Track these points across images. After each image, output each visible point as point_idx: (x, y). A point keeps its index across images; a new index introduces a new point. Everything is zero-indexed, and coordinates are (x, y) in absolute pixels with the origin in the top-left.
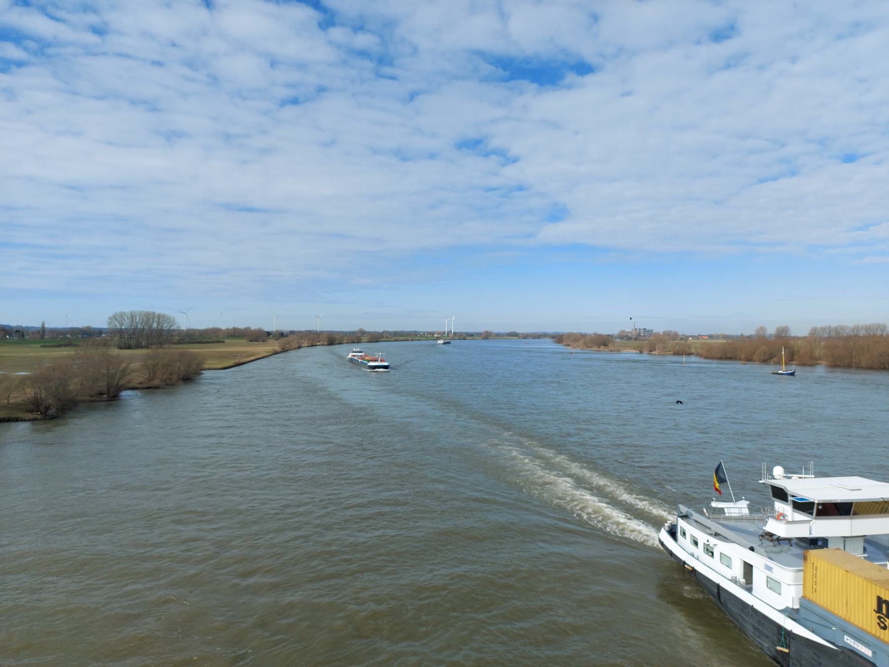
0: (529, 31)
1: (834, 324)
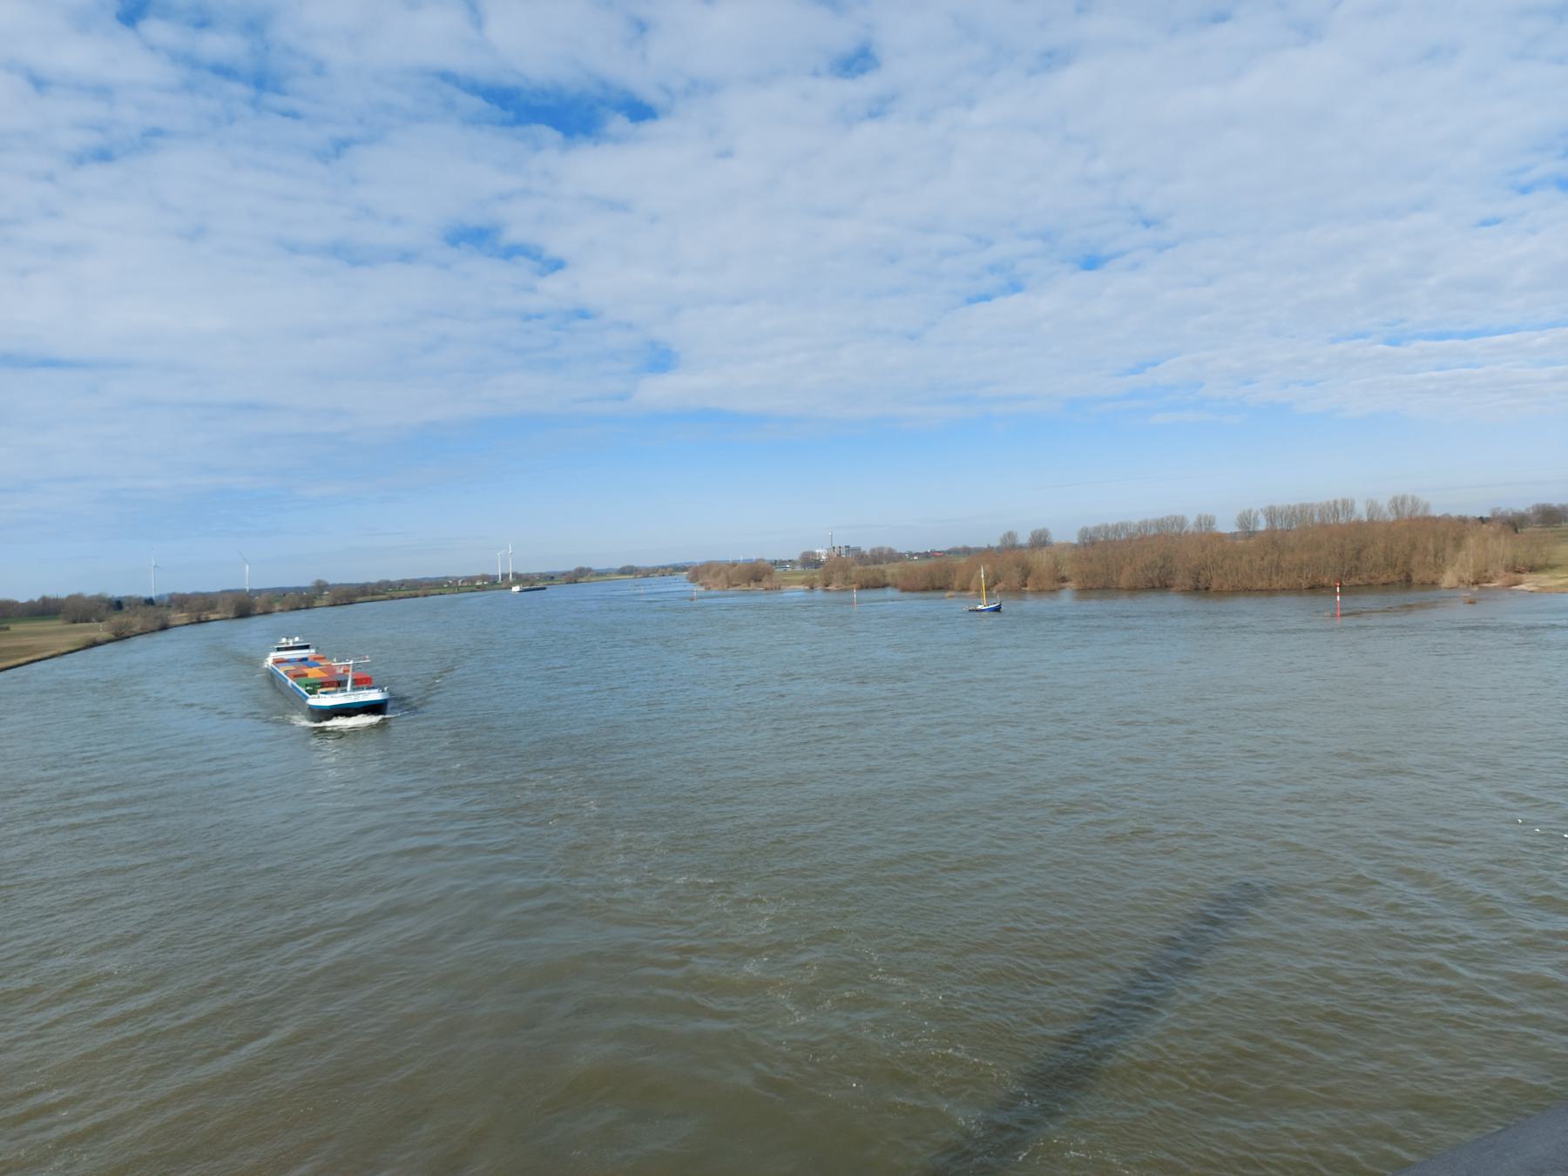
0: (533, 38)
1: (1112, 521)
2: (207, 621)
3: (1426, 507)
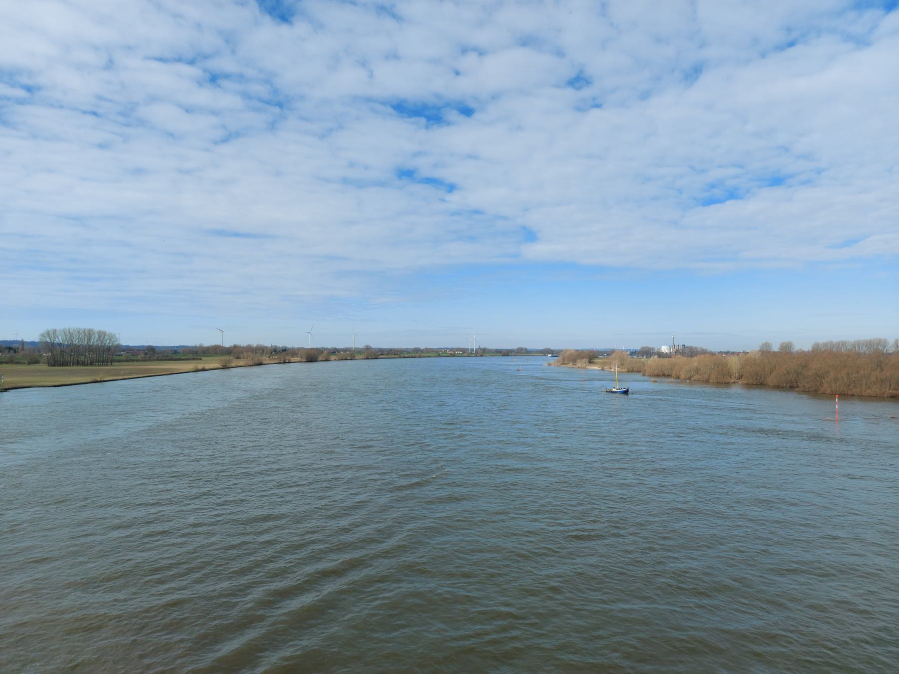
1: (835, 340)
2: (289, 362)
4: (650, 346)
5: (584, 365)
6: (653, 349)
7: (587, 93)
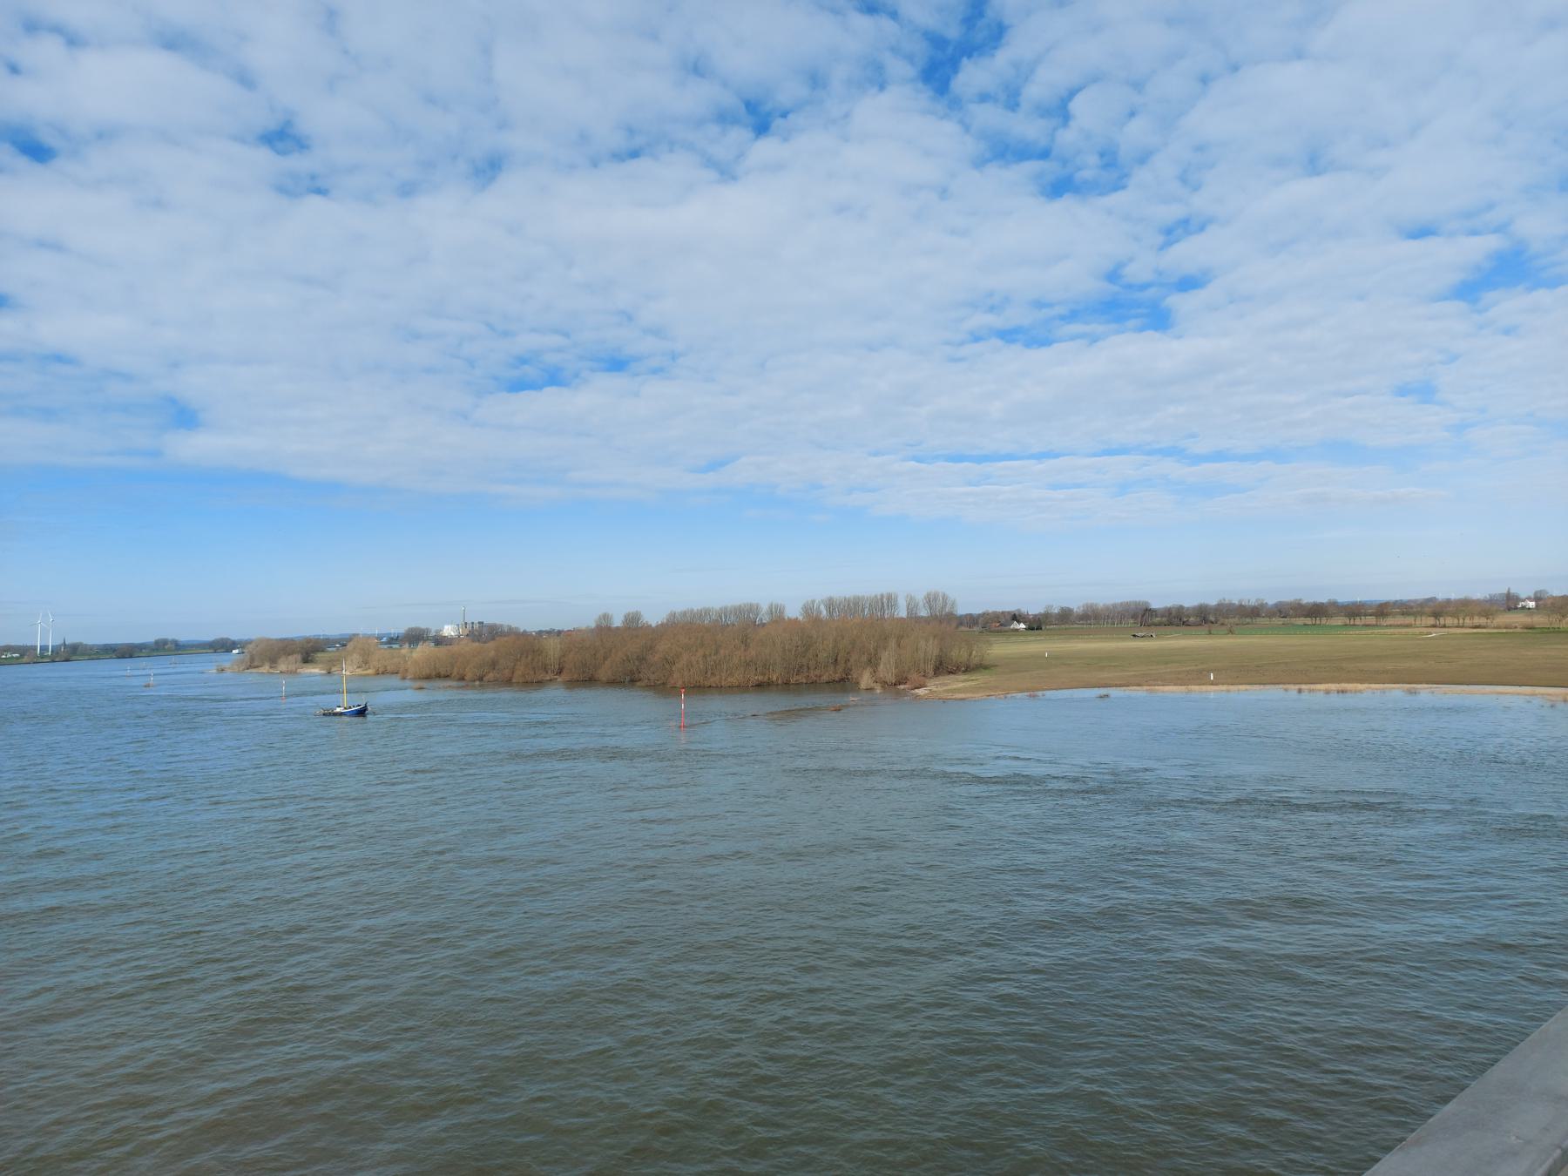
1: (697, 607)
3: (953, 604)
4: (423, 626)
5: (292, 667)
6: (428, 630)
7: (299, 163)
